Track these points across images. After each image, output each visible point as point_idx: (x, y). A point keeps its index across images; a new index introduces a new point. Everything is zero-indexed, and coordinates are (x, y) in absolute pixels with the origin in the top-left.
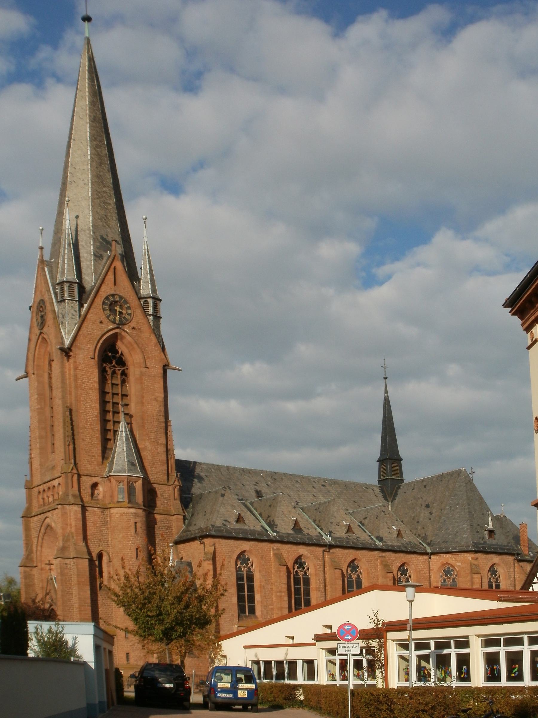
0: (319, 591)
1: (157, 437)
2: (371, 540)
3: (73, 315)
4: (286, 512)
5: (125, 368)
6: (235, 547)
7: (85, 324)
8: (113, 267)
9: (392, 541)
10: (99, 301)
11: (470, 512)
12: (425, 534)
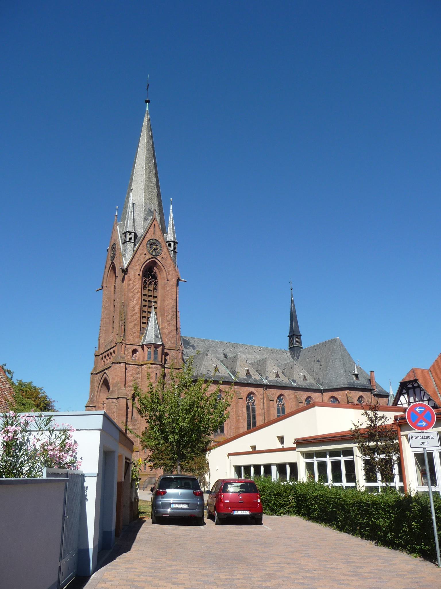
0: (261, 416)
1: (171, 321)
2: (289, 382)
3: (130, 250)
4: (242, 365)
5: (156, 281)
6: (213, 387)
7: (136, 255)
8: (153, 224)
9: (301, 383)
10: (145, 242)
11: (344, 363)
12: (319, 378)
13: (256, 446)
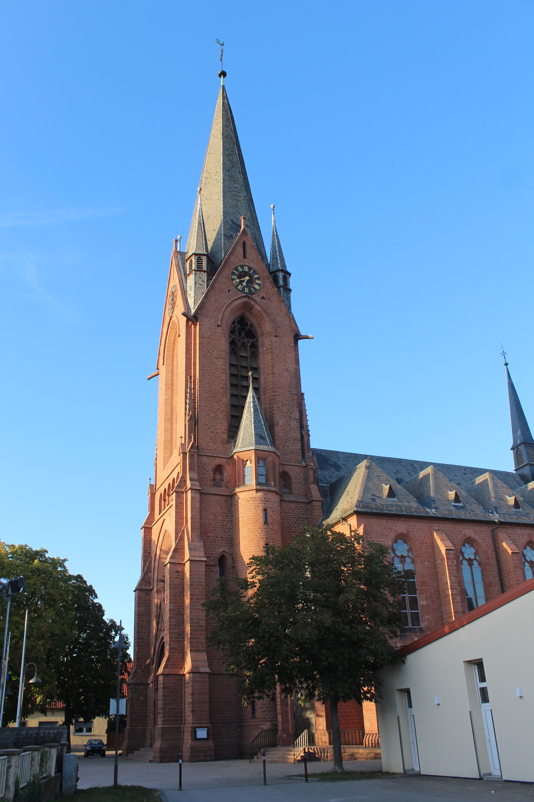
5: (255, 340)
13: (482, 659)
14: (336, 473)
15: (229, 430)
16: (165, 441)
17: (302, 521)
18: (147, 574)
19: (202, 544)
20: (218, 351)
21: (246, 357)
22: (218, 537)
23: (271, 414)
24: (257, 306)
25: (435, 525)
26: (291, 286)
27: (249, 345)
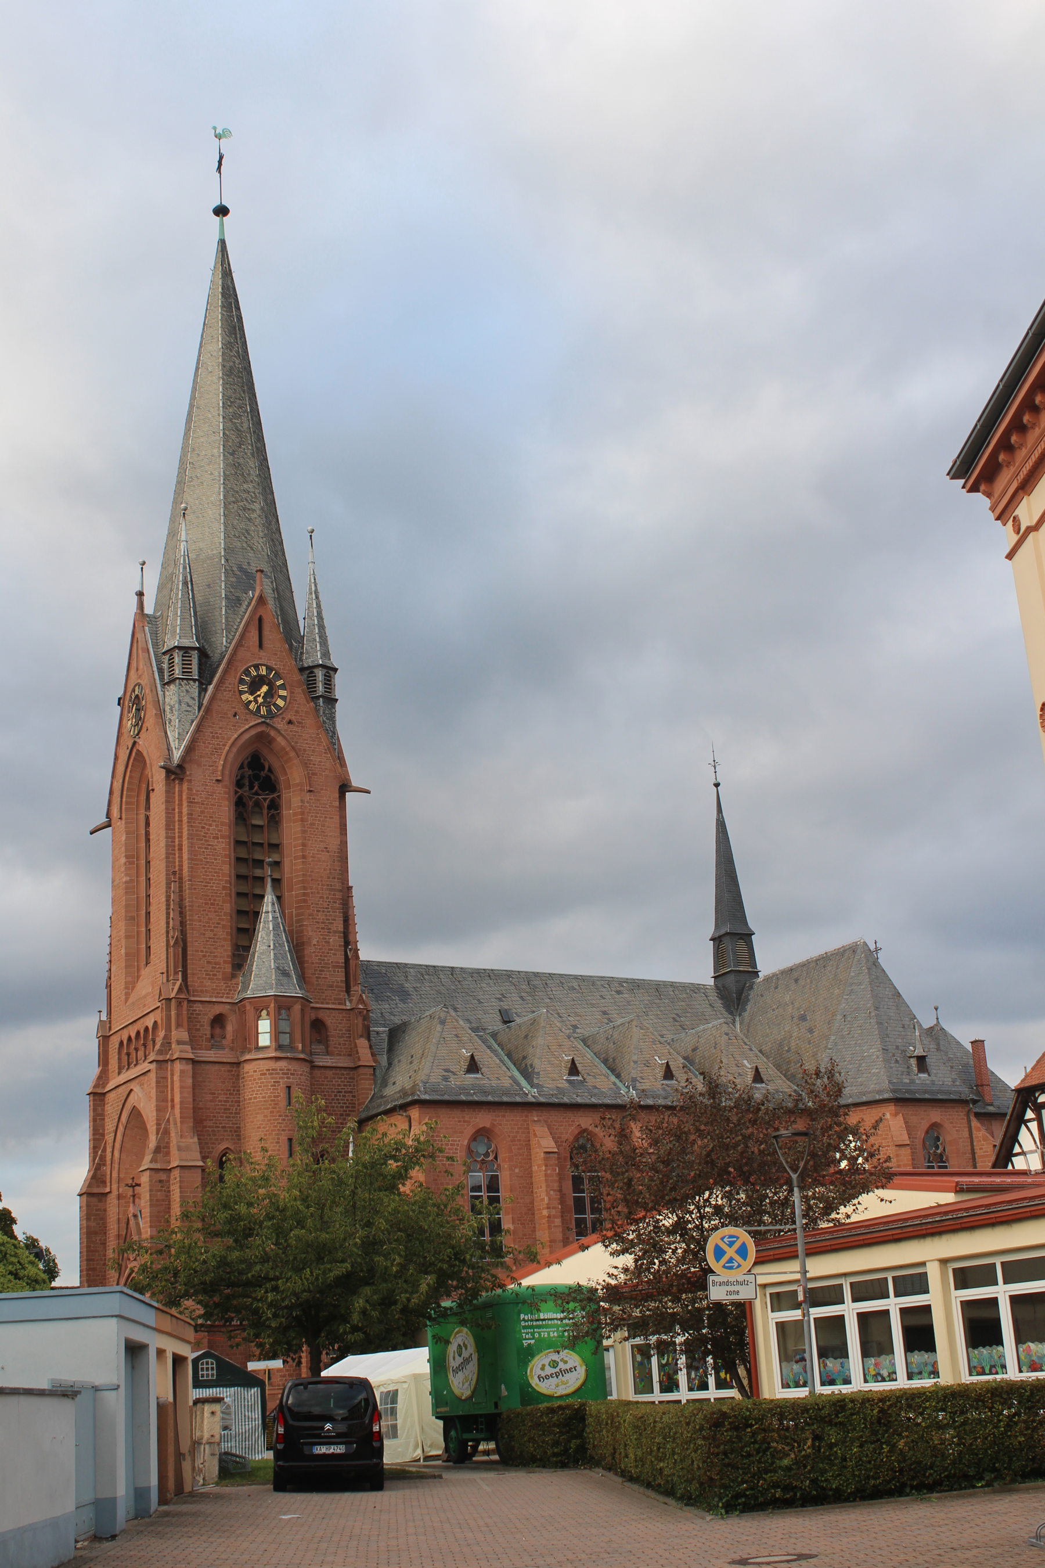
5: (275, 795)
14: (401, 1005)
15: (234, 955)
16: (127, 954)
17: (344, 1096)
18: (99, 1169)
19: (196, 1139)
20: (217, 826)
21: (261, 827)
22: (218, 1127)
23: (300, 926)
24: (279, 739)
25: (534, 1113)
26: (338, 693)
27: (266, 805)
